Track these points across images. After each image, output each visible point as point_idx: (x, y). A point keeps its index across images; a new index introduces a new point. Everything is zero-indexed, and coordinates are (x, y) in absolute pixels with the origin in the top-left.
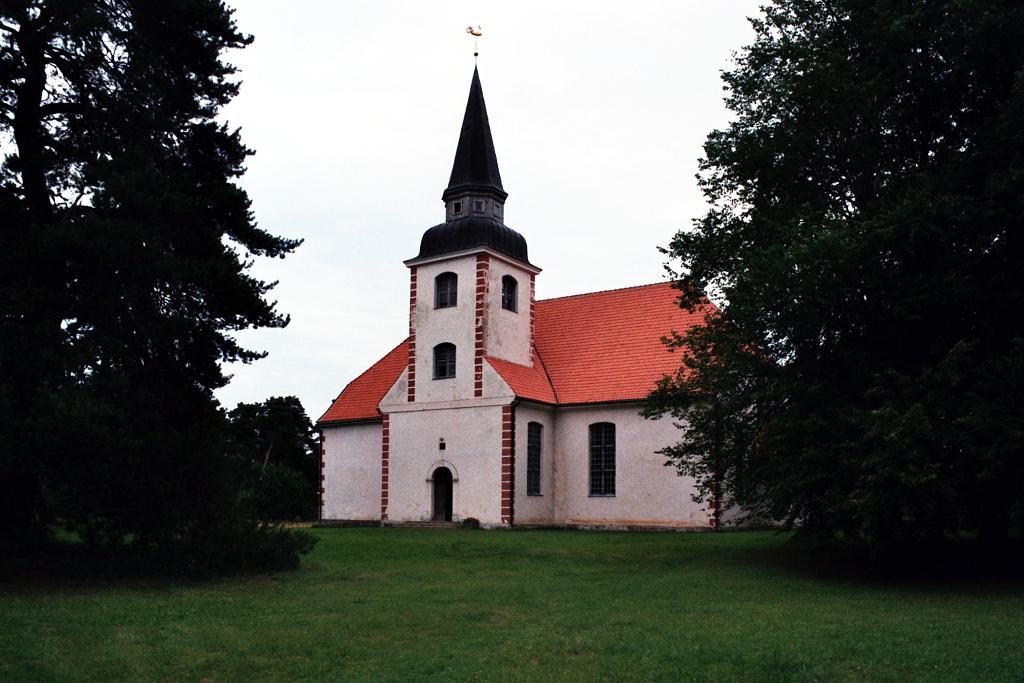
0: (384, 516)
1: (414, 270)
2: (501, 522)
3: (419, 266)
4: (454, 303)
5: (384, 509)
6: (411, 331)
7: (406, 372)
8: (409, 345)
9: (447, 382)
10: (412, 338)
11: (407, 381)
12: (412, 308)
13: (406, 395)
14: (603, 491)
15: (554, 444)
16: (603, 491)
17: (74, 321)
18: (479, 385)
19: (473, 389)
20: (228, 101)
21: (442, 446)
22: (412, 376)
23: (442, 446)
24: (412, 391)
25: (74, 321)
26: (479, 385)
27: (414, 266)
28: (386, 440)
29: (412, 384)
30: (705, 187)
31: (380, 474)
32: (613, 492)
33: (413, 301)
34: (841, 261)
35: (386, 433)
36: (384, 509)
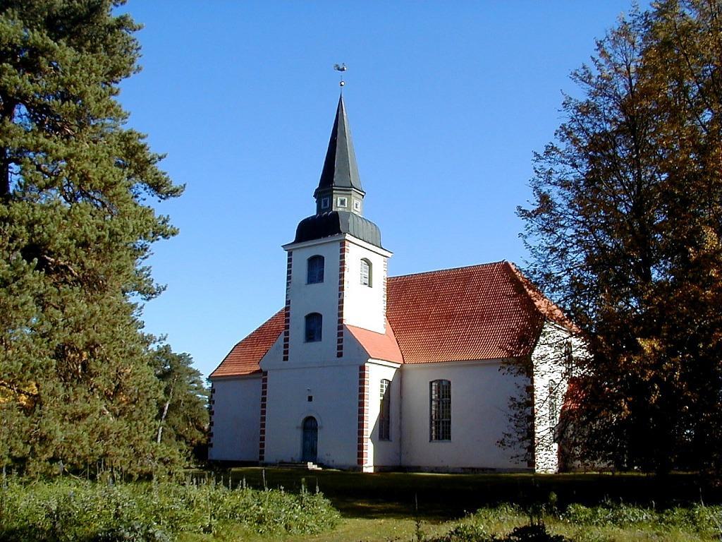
1: (290, 254)
2: (357, 463)
3: (294, 249)
4: (321, 279)
6: (288, 302)
7: (282, 336)
8: (286, 313)
9: (316, 287)
10: (287, 309)
11: (282, 343)
12: (288, 284)
14: (441, 438)
15: (401, 413)
16: (441, 438)
17: (45, 256)
18: (340, 348)
19: (336, 351)
20: (212, 444)
21: (310, 399)
22: (286, 340)
23: (310, 399)
24: (286, 352)
25: (45, 256)
26: (340, 348)
27: (290, 249)
28: (265, 387)
29: (286, 346)
30: (558, 364)
31: (259, 409)
32: (450, 438)
33: (289, 278)
34: (672, 298)
35: (265, 380)
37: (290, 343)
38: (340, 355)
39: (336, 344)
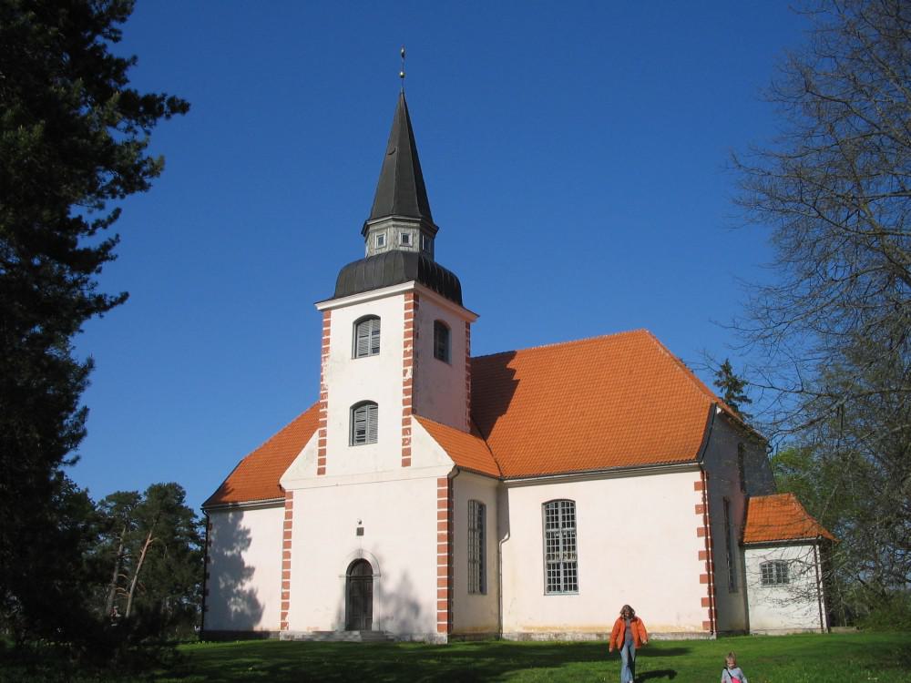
0: (284, 625)
5: (284, 615)
13: (315, 467)
14: (562, 588)
18: (407, 452)
21: (360, 532)
23: (360, 532)
24: (322, 462)
26: (407, 452)
36: (284, 615)
37: (293, 530)
38: (406, 463)
39: (401, 448)
